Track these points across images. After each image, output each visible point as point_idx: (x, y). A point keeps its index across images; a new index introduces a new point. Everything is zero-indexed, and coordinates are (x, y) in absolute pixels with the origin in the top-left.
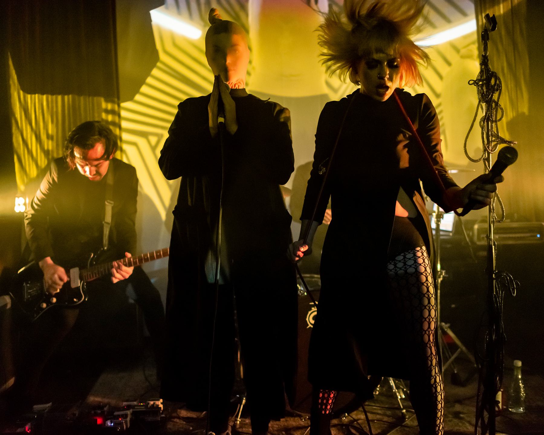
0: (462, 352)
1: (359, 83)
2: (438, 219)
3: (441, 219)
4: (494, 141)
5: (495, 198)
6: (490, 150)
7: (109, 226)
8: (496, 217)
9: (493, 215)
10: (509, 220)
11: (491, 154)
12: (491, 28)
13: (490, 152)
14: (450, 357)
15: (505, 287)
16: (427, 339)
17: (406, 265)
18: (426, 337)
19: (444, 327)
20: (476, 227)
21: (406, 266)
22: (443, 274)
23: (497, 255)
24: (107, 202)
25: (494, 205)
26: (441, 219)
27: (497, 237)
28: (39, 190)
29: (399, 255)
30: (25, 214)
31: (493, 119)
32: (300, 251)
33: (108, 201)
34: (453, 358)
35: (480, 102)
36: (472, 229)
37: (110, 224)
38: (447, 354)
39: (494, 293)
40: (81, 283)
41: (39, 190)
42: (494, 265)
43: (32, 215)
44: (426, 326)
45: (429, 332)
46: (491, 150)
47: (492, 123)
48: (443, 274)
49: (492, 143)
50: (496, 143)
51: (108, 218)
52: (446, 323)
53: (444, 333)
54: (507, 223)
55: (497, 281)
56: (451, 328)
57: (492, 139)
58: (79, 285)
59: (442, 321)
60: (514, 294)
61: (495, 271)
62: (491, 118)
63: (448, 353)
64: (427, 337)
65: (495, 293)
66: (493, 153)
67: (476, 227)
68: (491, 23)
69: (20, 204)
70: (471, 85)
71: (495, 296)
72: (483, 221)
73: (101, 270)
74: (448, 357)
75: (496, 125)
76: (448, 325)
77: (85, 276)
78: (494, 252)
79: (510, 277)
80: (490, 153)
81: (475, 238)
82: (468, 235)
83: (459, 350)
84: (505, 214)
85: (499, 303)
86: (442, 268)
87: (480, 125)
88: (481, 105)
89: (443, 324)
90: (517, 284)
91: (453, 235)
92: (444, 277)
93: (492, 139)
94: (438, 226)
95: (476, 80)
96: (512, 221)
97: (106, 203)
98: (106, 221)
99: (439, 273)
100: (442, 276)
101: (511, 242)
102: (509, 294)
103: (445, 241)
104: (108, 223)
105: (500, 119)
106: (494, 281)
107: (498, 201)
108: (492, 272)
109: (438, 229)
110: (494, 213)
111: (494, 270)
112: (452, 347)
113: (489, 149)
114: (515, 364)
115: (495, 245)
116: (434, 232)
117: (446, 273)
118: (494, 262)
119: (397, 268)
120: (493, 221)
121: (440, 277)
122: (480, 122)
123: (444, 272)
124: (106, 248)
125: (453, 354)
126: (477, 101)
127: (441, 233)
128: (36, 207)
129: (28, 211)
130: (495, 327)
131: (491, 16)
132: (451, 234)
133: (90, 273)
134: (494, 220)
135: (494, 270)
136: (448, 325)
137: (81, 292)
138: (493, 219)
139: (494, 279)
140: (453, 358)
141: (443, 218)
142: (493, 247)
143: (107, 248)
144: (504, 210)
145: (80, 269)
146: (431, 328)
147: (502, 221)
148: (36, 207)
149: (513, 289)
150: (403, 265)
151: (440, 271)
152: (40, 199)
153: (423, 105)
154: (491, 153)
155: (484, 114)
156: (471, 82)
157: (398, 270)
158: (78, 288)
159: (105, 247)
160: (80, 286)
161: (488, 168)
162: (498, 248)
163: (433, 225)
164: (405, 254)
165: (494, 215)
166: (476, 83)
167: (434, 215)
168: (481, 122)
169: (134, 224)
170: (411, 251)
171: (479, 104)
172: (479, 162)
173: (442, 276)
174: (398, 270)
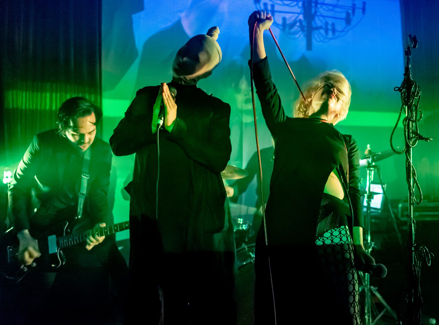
0: (387, 311)
1: (311, 94)
2: (369, 200)
3: (372, 199)
4: (414, 137)
5: (414, 184)
6: (411, 145)
7: (84, 197)
8: (415, 200)
9: (412, 198)
10: (426, 201)
11: (411, 148)
12: (413, 46)
13: (411, 146)
14: (377, 316)
15: (422, 258)
16: (353, 311)
17: (333, 235)
18: (352, 309)
19: (373, 290)
20: (400, 205)
21: (341, 235)
22: (373, 245)
23: (416, 230)
24: (83, 175)
25: (414, 190)
26: (372, 199)
27: (417, 214)
28: (22, 160)
29: (327, 231)
30: (9, 185)
31: (413, 119)
32: (360, 272)
33: (84, 174)
34: (380, 316)
35: (403, 105)
36: (397, 207)
37: (85, 195)
38: (375, 313)
39: (413, 263)
40: (58, 250)
41: (22, 160)
42: (414, 239)
43: (14, 185)
44: (351, 300)
45: (354, 304)
46: (412, 145)
47: (412, 123)
48: (373, 245)
49: (412, 139)
50: (415, 139)
51: (84, 190)
52: (374, 286)
53: (373, 295)
54: (424, 203)
55: (415, 253)
56: (378, 291)
57: (412, 136)
58: (57, 251)
59: (371, 285)
60: (429, 264)
61: (414, 244)
62: (412, 118)
63: (376, 312)
64: (353, 309)
65: (414, 263)
66: (413, 147)
67: (400, 205)
68: (413, 42)
69: (8, 176)
70: (396, 87)
71: (414, 266)
72: (406, 201)
73: (76, 238)
74: (376, 315)
75: (416, 124)
76: (376, 288)
77: (62, 244)
78: (413, 228)
79: (426, 250)
80: (411, 147)
81: (400, 215)
82: (394, 212)
83: (385, 310)
84: (422, 198)
85: (417, 272)
86: (372, 240)
87: (403, 124)
88: (404, 107)
89: (372, 287)
90: (431, 255)
91: (381, 212)
92: (373, 248)
93: (412, 136)
94: (369, 204)
95: (400, 88)
96: (429, 201)
97: (83, 176)
98: (81, 192)
99: (370, 244)
100: (371, 247)
101: (428, 219)
102: (424, 263)
103: (376, 217)
104: (83, 194)
105: (419, 120)
106: (413, 253)
107: (416, 186)
108: (412, 245)
109: (369, 207)
110: (414, 196)
111: (413, 243)
112: (378, 306)
113: (409, 143)
114: (430, 322)
115: (414, 222)
116: (365, 210)
117: (375, 245)
118: (413, 237)
119: (333, 236)
120: (413, 203)
121: (370, 248)
122: (403, 121)
123: (373, 243)
124: (79, 217)
125: (380, 312)
126: (401, 104)
127: (372, 210)
128: (18, 177)
129: (11, 182)
130: (414, 291)
131: (413, 36)
132: (380, 211)
133: (66, 241)
134: (413, 202)
135: (413, 243)
136: (376, 288)
137: (58, 258)
138: (413, 201)
139: (413, 251)
140: (380, 316)
141: (373, 198)
142: (413, 224)
143: (81, 217)
144: (422, 194)
145: (57, 237)
146: (356, 301)
147: (420, 203)
148: (18, 177)
149: (429, 260)
150: (338, 234)
151: (370, 243)
152: (22, 169)
153: (370, 256)
154: (412, 147)
155: (406, 115)
156: (397, 89)
157: (333, 238)
158: (55, 255)
159: (79, 216)
160: (57, 252)
161: (409, 159)
162: (418, 224)
163: (365, 204)
164: (332, 231)
165: (414, 198)
166: (400, 90)
167: (366, 195)
168: (404, 122)
169: (106, 194)
170: (337, 229)
171: (403, 107)
172: (402, 154)
173: (371, 247)
174: (333, 238)
